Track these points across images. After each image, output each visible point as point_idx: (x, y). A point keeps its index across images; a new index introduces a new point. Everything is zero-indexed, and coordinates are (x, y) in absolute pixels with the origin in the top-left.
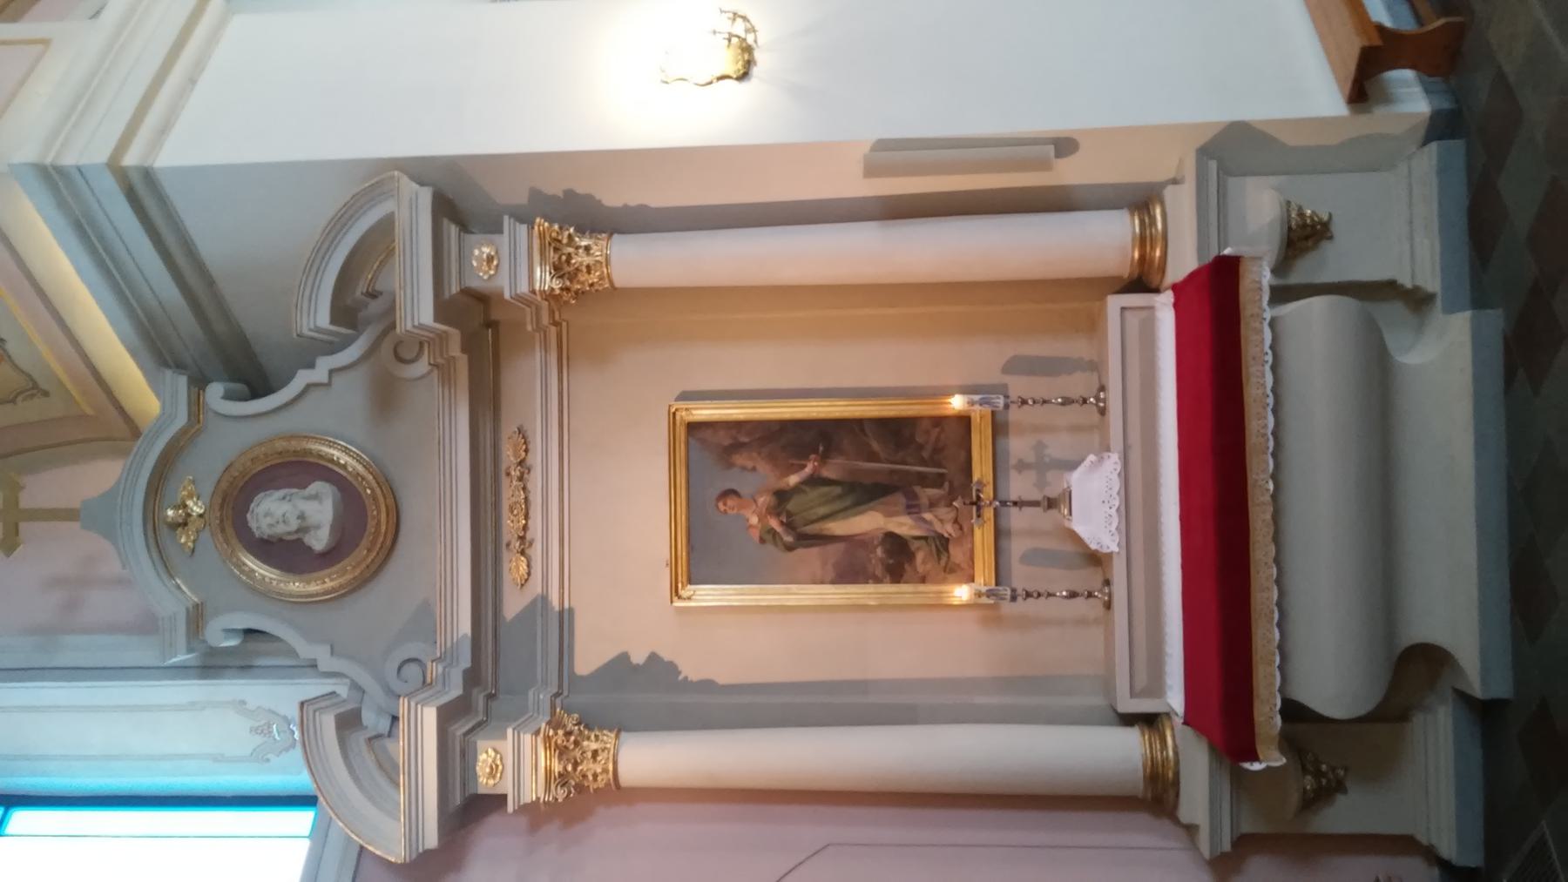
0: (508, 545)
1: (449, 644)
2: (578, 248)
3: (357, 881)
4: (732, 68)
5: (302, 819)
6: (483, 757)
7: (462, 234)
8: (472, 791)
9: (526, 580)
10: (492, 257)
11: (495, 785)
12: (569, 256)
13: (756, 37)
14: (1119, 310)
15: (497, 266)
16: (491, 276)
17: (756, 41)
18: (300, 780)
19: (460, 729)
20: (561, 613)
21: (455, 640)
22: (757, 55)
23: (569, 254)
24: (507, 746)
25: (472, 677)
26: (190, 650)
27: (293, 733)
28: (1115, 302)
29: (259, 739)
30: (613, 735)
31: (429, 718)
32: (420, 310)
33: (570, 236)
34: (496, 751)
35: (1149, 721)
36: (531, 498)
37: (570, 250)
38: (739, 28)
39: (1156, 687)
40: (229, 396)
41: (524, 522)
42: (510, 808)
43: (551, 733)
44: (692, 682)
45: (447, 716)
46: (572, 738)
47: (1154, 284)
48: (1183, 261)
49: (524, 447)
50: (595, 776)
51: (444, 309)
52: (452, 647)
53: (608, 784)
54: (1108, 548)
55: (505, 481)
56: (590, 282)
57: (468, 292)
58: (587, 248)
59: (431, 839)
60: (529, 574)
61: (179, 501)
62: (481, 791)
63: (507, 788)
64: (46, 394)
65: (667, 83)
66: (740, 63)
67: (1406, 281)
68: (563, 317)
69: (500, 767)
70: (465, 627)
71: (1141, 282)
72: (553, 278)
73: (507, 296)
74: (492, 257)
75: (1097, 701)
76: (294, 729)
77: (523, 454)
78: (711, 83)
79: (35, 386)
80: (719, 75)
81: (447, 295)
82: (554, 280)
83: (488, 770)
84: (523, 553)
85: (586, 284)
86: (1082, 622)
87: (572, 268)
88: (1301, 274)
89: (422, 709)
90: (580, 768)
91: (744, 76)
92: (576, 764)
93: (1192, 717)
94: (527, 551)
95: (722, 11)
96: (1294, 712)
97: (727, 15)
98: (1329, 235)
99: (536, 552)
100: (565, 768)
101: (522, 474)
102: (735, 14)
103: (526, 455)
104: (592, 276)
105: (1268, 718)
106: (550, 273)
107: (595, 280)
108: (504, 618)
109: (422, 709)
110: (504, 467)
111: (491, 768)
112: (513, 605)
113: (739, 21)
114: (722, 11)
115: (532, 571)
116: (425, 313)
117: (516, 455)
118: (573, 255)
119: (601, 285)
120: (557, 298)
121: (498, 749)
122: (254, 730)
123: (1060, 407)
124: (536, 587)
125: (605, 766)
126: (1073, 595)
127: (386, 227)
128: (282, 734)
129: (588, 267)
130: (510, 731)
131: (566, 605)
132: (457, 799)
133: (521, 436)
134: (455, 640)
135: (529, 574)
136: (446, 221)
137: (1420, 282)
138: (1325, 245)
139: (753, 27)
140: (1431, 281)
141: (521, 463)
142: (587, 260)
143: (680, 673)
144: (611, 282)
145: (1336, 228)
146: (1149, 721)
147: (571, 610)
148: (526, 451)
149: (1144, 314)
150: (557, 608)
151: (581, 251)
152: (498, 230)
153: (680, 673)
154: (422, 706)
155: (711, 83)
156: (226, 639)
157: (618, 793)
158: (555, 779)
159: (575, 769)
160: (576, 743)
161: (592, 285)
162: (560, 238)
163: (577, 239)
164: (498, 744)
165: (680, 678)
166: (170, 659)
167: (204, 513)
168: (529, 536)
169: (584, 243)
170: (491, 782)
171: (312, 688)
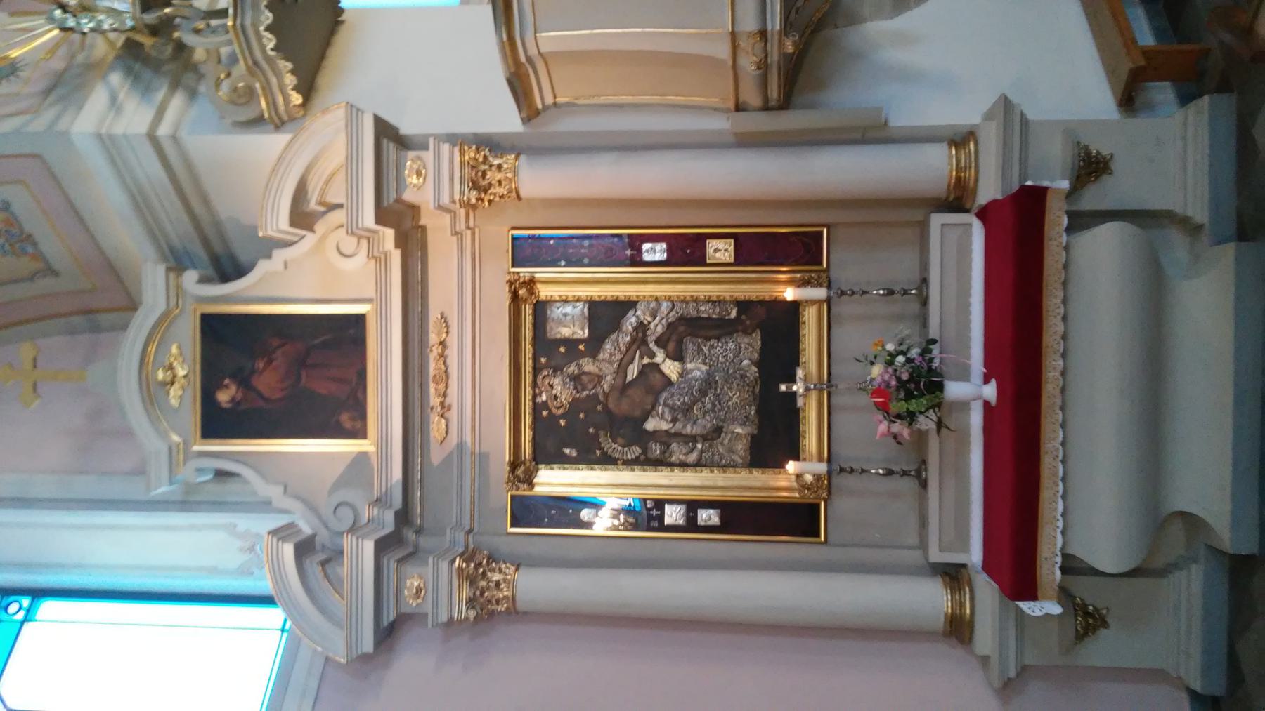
0: (432, 408)
1: (384, 490)
2: (491, 166)
5: (273, 616)
7: (399, 151)
11: (418, 605)
14: (940, 227)
18: (264, 585)
19: (390, 563)
21: (371, 517)
25: (403, 517)
26: (171, 483)
29: (246, 557)
30: (513, 568)
31: (369, 547)
33: (485, 157)
37: (486, 167)
39: (965, 547)
40: (203, 280)
43: (464, 565)
45: (382, 547)
46: (481, 570)
47: (968, 206)
48: (989, 190)
52: (387, 490)
53: (507, 608)
54: (927, 425)
58: (499, 167)
61: (167, 363)
63: (428, 608)
67: (1178, 209)
72: (471, 189)
75: (914, 556)
77: (444, 335)
81: (385, 204)
82: (472, 191)
84: (442, 416)
87: (486, 182)
88: (1092, 199)
93: (988, 566)
94: (446, 414)
96: (1071, 566)
98: (1110, 171)
99: (453, 415)
100: (474, 594)
103: (447, 336)
104: (500, 606)
105: (1050, 571)
106: (468, 186)
115: (450, 430)
117: (439, 334)
130: (430, 560)
133: (443, 320)
135: (447, 433)
136: (385, 141)
137: (1190, 213)
138: (1105, 177)
140: (1199, 212)
142: (499, 176)
145: (1114, 165)
146: (953, 575)
148: (447, 333)
152: (426, 148)
154: (362, 540)
157: (515, 613)
163: (491, 159)
166: (156, 489)
167: (188, 373)
169: (496, 162)
171: (262, 524)
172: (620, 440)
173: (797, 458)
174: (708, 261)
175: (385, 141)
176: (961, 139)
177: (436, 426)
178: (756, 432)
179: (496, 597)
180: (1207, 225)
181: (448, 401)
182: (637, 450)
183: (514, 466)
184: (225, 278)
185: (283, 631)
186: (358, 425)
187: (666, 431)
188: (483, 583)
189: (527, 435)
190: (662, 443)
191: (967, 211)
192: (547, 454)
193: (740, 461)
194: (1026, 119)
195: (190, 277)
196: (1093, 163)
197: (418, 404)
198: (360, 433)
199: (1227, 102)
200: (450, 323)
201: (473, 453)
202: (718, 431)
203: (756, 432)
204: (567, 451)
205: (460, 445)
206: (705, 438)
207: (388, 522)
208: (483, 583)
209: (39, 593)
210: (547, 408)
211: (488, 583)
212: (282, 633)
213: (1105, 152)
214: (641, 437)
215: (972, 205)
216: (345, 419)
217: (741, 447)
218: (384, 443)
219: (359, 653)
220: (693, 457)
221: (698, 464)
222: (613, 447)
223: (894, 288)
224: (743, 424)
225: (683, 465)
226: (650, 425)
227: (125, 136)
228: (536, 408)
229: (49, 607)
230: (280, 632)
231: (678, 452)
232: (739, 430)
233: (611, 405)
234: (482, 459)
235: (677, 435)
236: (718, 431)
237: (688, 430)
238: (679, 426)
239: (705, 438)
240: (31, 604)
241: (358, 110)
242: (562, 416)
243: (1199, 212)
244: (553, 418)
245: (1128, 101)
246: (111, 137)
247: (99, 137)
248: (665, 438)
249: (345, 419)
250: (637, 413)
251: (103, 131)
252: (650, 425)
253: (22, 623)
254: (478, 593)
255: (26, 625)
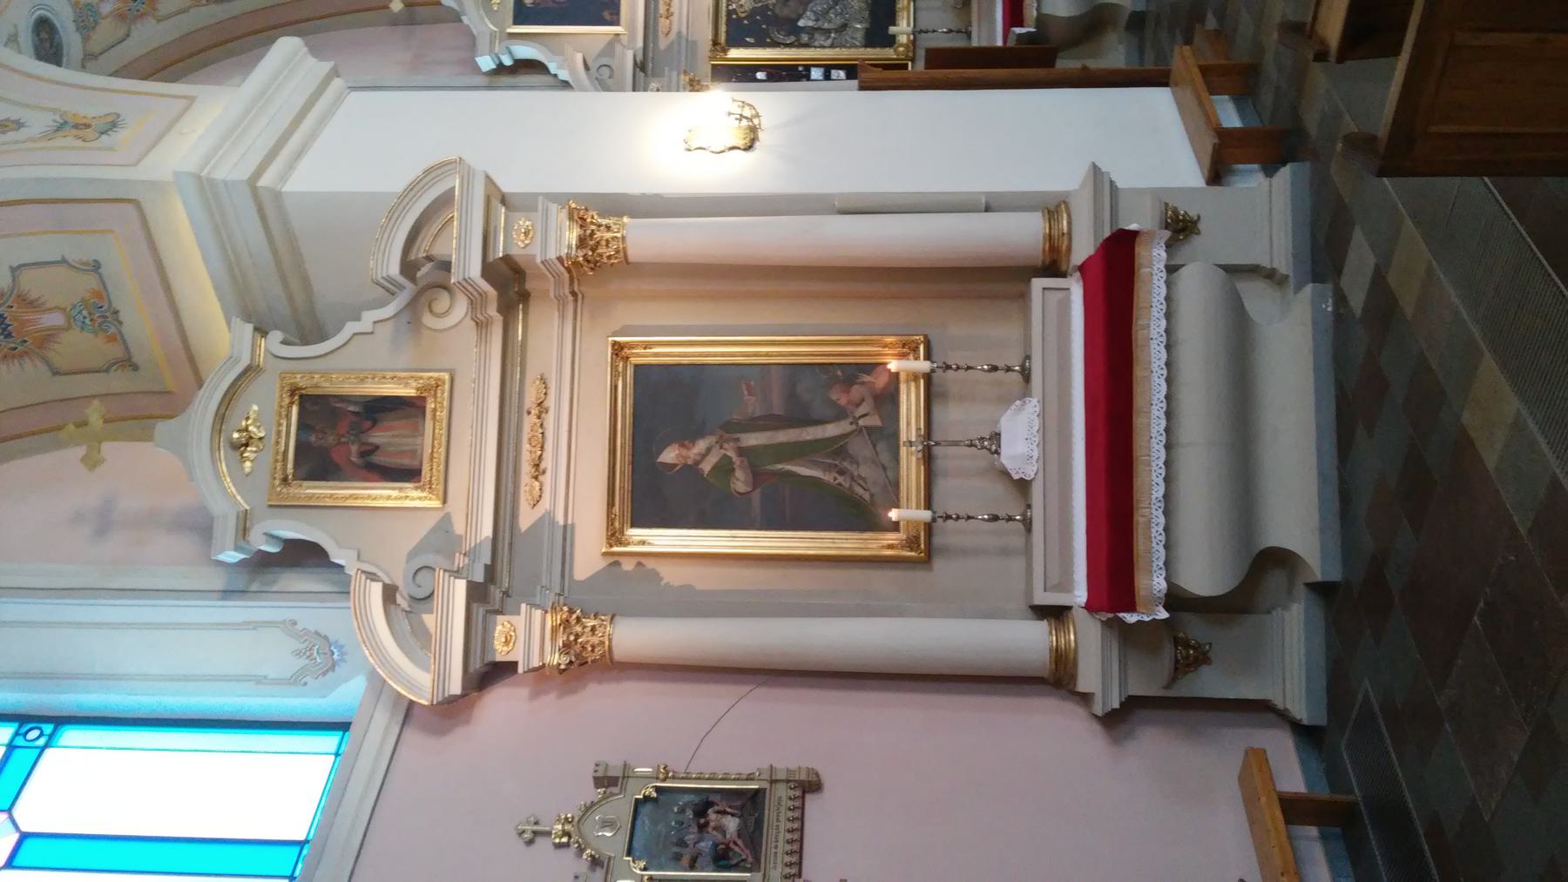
3: (352, 881)
4: (741, 143)
5: (330, 741)
6: (499, 628)
8: (489, 659)
9: (538, 501)
10: (529, 230)
12: (593, 233)
13: (760, 121)
15: (532, 238)
16: (527, 245)
17: (759, 124)
20: (565, 527)
22: (761, 135)
23: (593, 231)
24: (519, 621)
25: (491, 571)
27: (333, 653)
28: (1038, 284)
29: (303, 662)
31: (460, 587)
32: (470, 266)
34: (509, 622)
35: (1056, 614)
36: (546, 434)
38: (747, 112)
39: (1066, 585)
40: (285, 342)
41: (540, 452)
42: (520, 670)
44: (672, 586)
45: (476, 594)
49: (544, 390)
50: (593, 647)
51: (488, 270)
53: (603, 656)
55: (526, 417)
56: (608, 254)
57: (507, 259)
59: (455, 687)
60: (540, 496)
62: (499, 658)
63: (517, 655)
64: (135, 368)
65: (689, 150)
66: (748, 139)
68: (582, 289)
69: (514, 638)
70: (517, 389)
71: (1053, 268)
73: (538, 260)
74: (529, 230)
76: (335, 651)
78: (723, 152)
79: (129, 359)
80: (730, 146)
83: (503, 640)
85: (604, 257)
86: (1005, 552)
89: (454, 581)
90: (580, 640)
91: (749, 148)
92: (577, 636)
95: (734, 100)
97: (737, 103)
101: (541, 412)
102: (743, 102)
107: (612, 253)
108: (520, 529)
109: (454, 581)
110: (526, 408)
111: (506, 637)
112: (527, 518)
113: (747, 108)
114: (734, 100)
116: (475, 270)
118: (595, 231)
119: (616, 258)
120: (576, 263)
121: (512, 622)
122: (298, 654)
123: (989, 374)
124: (546, 503)
125: (601, 639)
126: (995, 518)
127: (446, 200)
128: (322, 656)
129: (607, 241)
131: (570, 522)
132: (476, 664)
134: (478, 541)
139: (758, 113)
140: (1282, 261)
141: (540, 404)
142: (608, 235)
143: (662, 579)
144: (626, 256)
145: (1201, 226)
146: (1056, 614)
147: (573, 526)
149: (1060, 295)
150: (561, 523)
151: (602, 228)
153: (662, 579)
155: (723, 152)
156: (267, 543)
157: (625, 267)
158: (559, 650)
159: (576, 640)
160: (578, 619)
161: (609, 257)
162: (585, 217)
164: (513, 619)
165: (663, 583)
168: (543, 466)
170: (505, 649)
172: (782, 33)
173: (898, 507)
174: (822, 69)
175: (475, 606)
176: (1054, 207)
177: (663, 22)
178: (868, 27)
179: (591, 643)
180: (1291, 274)
181: (672, 10)
182: (792, 39)
183: (715, 43)
184: (305, 341)
185: (337, 754)
186: (615, 17)
187: (812, 27)
188: (578, 629)
189: (723, 28)
190: (808, 33)
191: (1064, 275)
192: (736, 40)
193: (858, 44)
194: (1116, 186)
195: (276, 336)
196: (1181, 221)
197: (513, 433)
198: (617, 23)
199: (1305, 168)
200: (549, 385)
201: (687, 40)
202: (844, 27)
203: (868, 27)
204: (748, 39)
205: (679, 33)
206: (837, 31)
207: (479, 577)
208: (578, 629)
209: (61, 721)
210: (737, 14)
211: (583, 629)
212: (336, 757)
213: (1193, 213)
214: (796, 31)
215: (1068, 267)
216: (606, 15)
217: (860, 36)
218: (631, 27)
219: (446, 695)
220: (829, 42)
221: (832, 46)
222: (780, 37)
223: (998, 364)
224: (861, 22)
225: (822, 47)
226: (801, 23)
227: (225, 183)
228: (729, 13)
229: (70, 734)
230: (333, 757)
231: (819, 39)
232: (859, 26)
233: (777, 11)
234: (692, 46)
235: (819, 29)
236: (844, 27)
237: (826, 26)
238: (820, 23)
239: (837, 31)
240: (55, 730)
241: (393, 294)
242: (745, 18)
243: (1282, 261)
244: (740, 20)
245: (1217, 175)
246: (212, 182)
247: (198, 178)
248: (811, 31)
249: (606, 15)
250: (794, 16)
251: (204, 174)
252: (801, 23)
253: (43, 749)
254: (572, 638)
255: (48, 752)
